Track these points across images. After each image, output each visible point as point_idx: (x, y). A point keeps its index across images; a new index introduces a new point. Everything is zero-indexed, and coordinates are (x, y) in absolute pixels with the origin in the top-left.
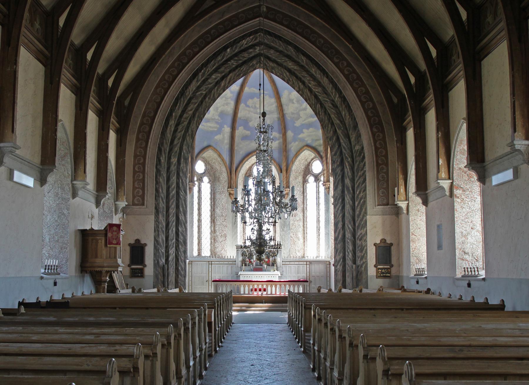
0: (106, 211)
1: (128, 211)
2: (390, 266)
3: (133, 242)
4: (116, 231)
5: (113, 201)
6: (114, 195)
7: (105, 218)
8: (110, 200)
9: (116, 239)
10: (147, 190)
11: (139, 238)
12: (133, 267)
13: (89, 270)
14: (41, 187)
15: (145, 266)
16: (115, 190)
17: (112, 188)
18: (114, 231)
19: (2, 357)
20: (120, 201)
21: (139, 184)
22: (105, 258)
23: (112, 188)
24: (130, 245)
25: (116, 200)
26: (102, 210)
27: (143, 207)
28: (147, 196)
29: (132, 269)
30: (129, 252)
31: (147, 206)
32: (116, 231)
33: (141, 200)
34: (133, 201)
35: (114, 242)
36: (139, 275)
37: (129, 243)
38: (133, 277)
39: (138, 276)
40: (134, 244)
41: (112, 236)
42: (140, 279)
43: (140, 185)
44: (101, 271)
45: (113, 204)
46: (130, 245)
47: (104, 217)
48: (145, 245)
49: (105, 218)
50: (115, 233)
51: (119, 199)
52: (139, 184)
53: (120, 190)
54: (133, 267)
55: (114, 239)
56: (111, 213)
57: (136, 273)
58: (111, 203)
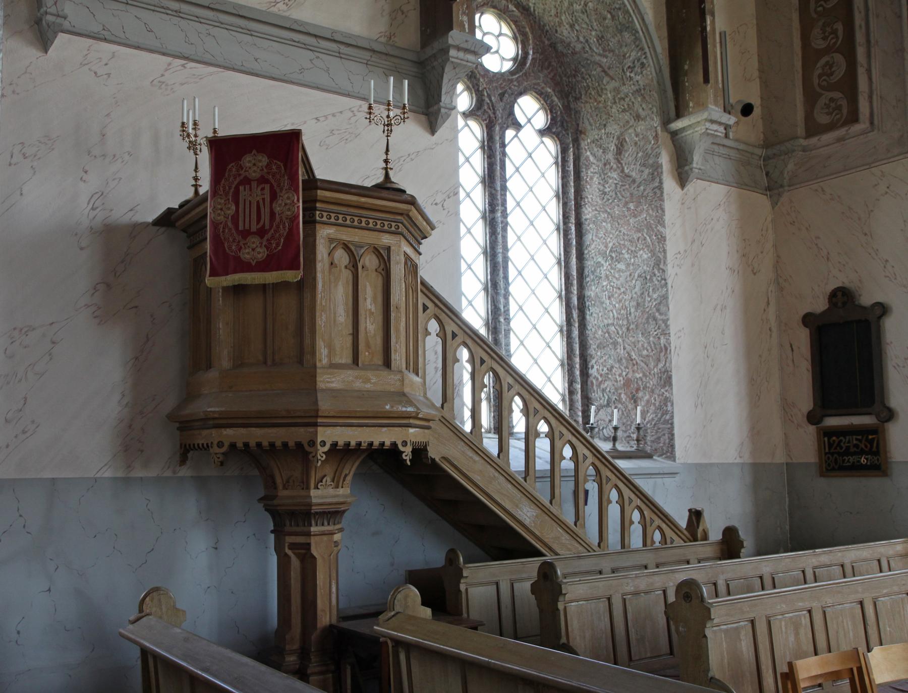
0: (634, 174)
1: (791, 166)
2: (878, 417)
3: (820, 305)
4: (262, 180)
5: (656, 122)
6: (662, 92)
7: (632, 206)
8: (644, 119)
9: (261, 233)
10: (868, 41)
11: (847, 284)
12: (832, 422)
13: (220, 444)
14: (46, 51)
15: (890, 415)
16: (659, 72)
17: (643, 65)
18: (247, 181)
19: (415, 689)
20: (690, 114)
21: (828, 29)
22: (226, 364)
23: (643, 65)
24: (808, 320)
25: (673, 113)
26: (614, 175)
27: (856, 128)
28: (869, 71)
29: (828, 434)
30: (808, 355)
31: (872, 123)
32: (262, 180)
33: (844, 103)
34: (809, 117)
35: (246, 255)
36: (863, 460)
37: (808, 310)
38: (833, 469)
39: (857, 469)
40: (824, 313)
41: (235, 219)
42: (872, 484)
43: (834, 32)
44: (394, 444)
45: (656, 137)
46: (808, 320)
47: (627, 203)
48: (878, 312)
49: (632, 206)
50: (255, 195)
51: (688, 106)
52: (828, 29)
53: (686, 67)
54: (832, 422)
55: (246, 234)
56: (653, 179)
57: (847, 452)
58: (650, 135)
